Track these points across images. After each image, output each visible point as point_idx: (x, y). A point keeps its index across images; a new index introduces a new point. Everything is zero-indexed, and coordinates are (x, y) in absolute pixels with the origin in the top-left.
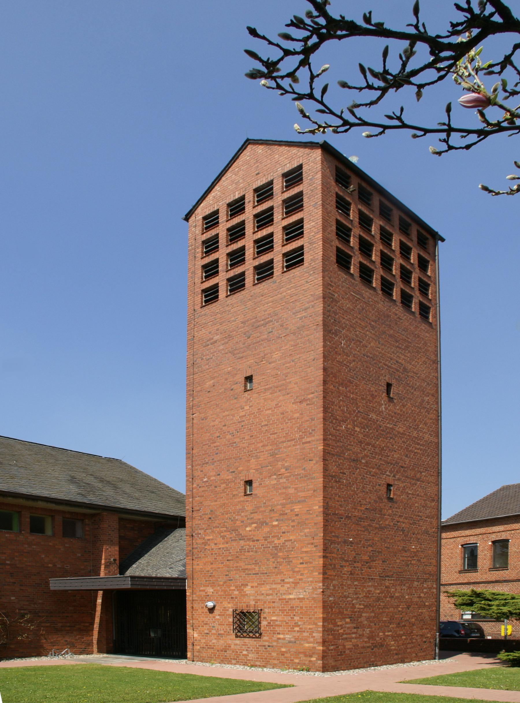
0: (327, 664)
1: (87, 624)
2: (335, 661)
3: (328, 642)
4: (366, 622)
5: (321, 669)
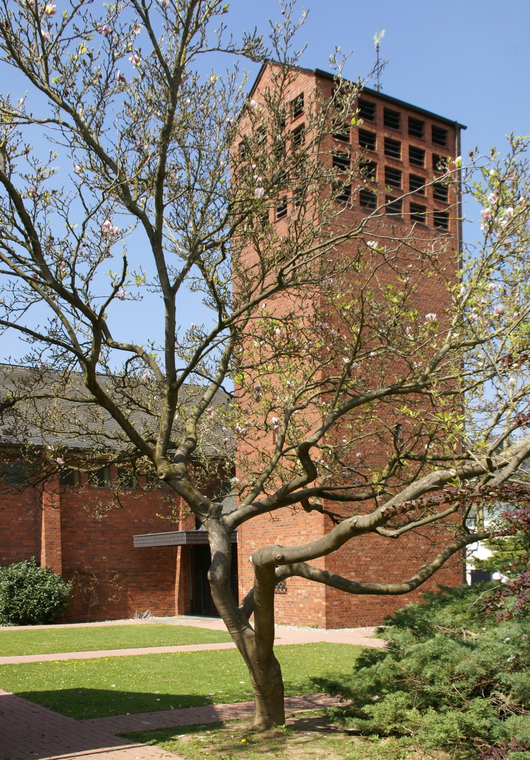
0: (332, 621)
1: (169, 583)
2: (340, 617)
3: (331, 597)
4: (373, 576)
5: (325, 626)
